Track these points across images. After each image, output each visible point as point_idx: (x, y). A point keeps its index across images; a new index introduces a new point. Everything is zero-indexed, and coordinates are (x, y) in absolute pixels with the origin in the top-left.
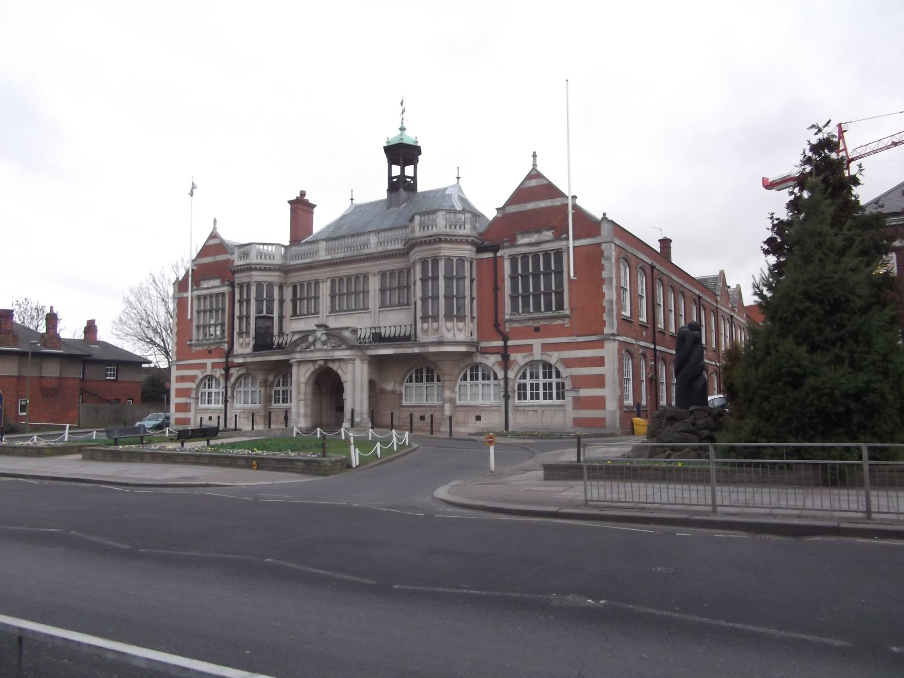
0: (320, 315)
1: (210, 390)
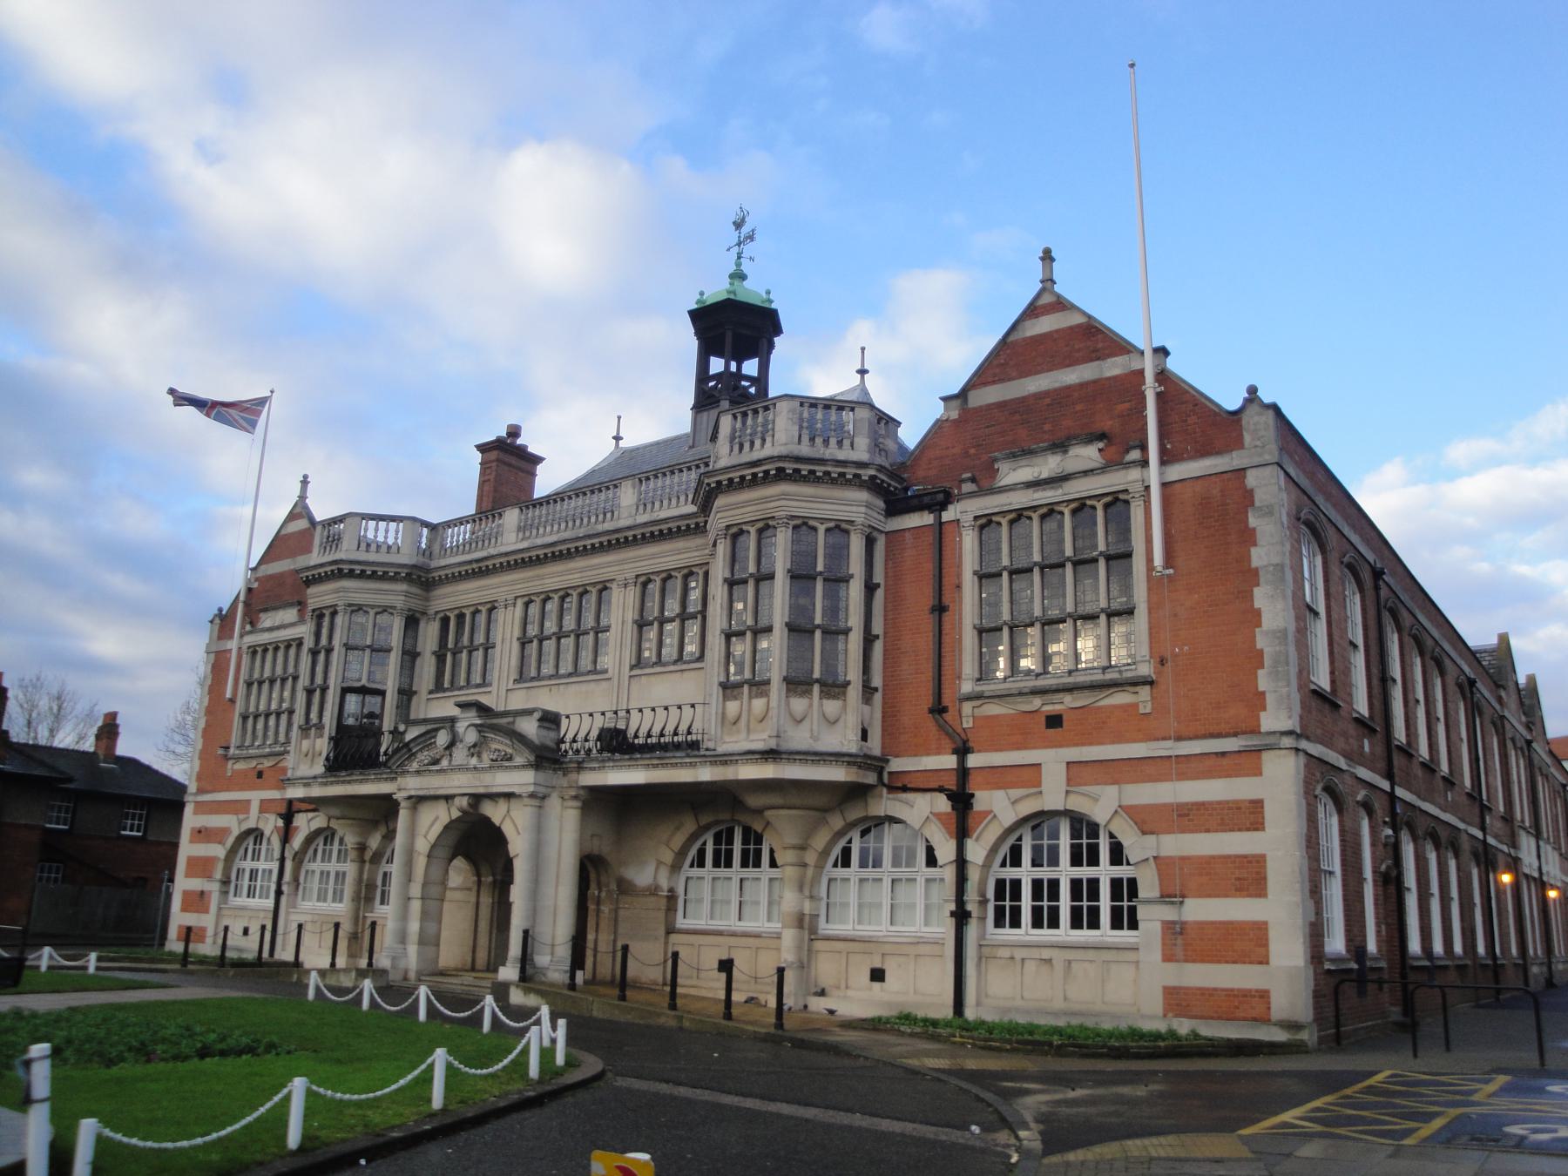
0: (494, 689)
1: (255, 865)
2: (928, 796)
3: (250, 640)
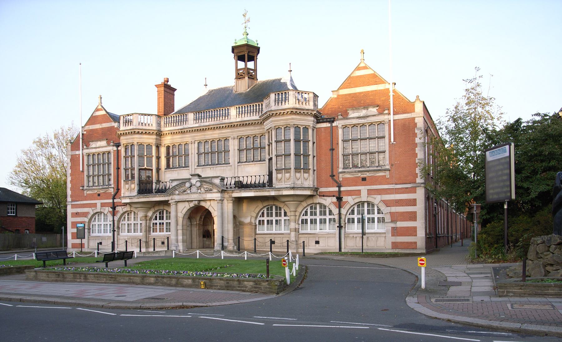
2: (330, 198)
3: (86, 151)
